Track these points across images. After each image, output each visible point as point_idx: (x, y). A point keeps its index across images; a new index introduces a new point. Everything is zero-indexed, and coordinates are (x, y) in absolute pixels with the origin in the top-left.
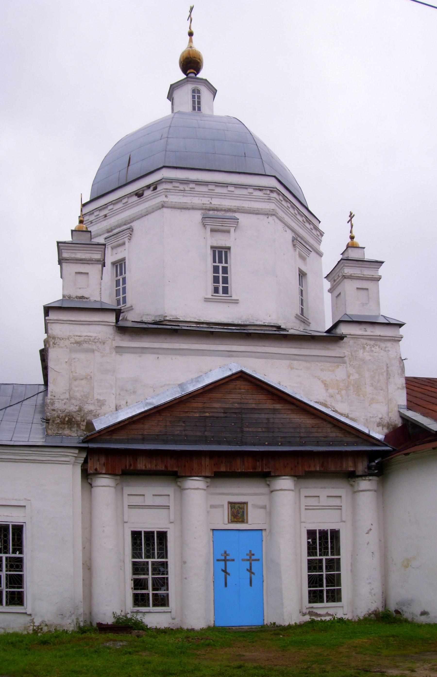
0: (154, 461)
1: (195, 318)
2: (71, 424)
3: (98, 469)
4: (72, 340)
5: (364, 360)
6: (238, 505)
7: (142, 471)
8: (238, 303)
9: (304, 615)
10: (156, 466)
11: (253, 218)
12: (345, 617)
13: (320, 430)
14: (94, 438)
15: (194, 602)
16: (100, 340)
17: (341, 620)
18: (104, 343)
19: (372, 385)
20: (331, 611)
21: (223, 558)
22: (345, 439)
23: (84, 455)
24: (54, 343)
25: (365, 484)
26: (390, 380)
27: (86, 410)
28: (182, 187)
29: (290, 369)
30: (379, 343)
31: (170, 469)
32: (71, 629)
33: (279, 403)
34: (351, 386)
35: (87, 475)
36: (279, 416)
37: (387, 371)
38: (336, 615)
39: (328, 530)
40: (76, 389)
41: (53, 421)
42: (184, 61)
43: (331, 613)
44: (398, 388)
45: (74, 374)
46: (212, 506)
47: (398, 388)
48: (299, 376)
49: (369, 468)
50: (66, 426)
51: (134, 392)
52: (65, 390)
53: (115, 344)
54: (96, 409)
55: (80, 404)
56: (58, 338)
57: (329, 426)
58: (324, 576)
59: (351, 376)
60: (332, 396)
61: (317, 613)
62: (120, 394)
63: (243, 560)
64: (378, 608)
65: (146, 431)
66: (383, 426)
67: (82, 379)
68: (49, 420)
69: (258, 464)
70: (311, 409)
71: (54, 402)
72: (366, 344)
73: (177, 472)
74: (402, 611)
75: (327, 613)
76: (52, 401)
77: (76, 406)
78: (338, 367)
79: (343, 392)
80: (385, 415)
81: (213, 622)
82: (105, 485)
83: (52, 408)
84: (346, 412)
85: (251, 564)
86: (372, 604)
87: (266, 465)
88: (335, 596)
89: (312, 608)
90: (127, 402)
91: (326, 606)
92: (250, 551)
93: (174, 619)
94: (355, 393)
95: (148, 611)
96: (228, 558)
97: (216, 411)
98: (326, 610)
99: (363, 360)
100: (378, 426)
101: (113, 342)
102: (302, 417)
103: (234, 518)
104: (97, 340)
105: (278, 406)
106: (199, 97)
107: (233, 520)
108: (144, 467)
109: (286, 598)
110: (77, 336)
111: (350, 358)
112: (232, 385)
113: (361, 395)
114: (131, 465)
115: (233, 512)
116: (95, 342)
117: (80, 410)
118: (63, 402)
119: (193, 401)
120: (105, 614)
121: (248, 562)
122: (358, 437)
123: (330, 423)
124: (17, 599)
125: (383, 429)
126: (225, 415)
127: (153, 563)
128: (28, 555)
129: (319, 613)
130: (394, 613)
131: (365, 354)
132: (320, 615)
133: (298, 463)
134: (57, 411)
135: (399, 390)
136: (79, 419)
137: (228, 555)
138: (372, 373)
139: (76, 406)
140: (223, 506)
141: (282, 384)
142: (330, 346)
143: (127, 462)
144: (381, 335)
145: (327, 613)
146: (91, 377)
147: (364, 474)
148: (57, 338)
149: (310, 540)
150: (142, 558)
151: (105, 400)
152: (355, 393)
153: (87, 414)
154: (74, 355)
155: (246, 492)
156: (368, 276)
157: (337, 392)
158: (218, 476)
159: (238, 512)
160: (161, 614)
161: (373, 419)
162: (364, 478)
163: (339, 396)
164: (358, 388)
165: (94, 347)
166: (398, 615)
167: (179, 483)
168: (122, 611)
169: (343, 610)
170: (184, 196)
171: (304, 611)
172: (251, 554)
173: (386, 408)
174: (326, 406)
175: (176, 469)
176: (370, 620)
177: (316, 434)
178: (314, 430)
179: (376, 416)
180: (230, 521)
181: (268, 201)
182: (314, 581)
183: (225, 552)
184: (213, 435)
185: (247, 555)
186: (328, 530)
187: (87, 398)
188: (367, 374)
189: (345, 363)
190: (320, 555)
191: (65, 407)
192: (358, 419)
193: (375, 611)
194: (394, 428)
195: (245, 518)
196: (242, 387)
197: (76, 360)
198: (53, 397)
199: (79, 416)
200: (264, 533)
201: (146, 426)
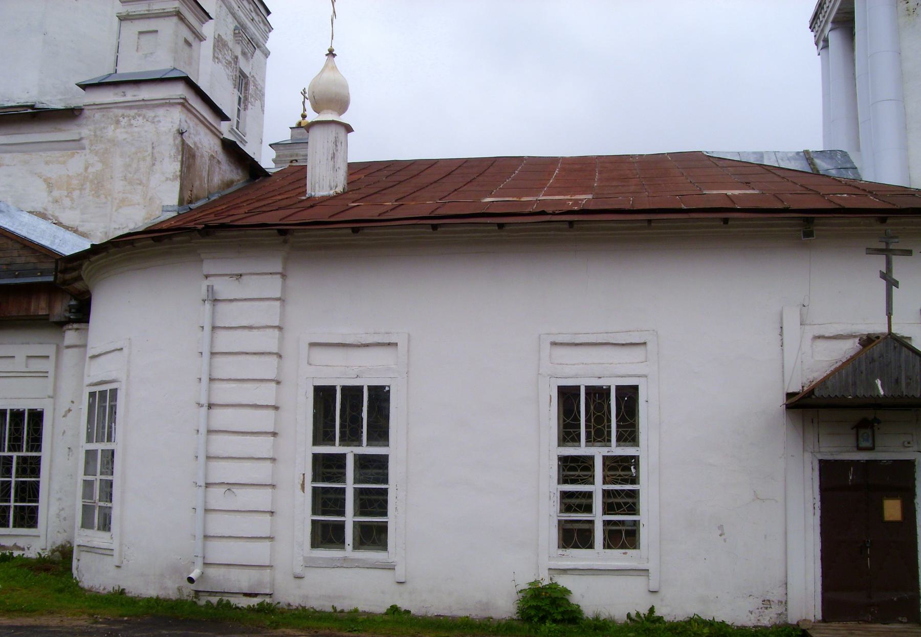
19: (125, 178)
20: (21, 543)
30: (144, 111)
44: (167, 179)
47: (167, 179)
48: (9, 176)
58: (13, 485)
78: (73, 155)
79: (76, 194)
99: (113, 142)
113: (102, 196)
124: (28, 518)
128: (397, 450)
131: (118, 130)
135: (169, 182)
138: (128, 160)
142: (63, 126)
145: (15, 545)
163: (68, 199)
164: (98, 185)
182: (327, 501)
189: (84, 148)
190: (10, 450)
193: (63, 546)
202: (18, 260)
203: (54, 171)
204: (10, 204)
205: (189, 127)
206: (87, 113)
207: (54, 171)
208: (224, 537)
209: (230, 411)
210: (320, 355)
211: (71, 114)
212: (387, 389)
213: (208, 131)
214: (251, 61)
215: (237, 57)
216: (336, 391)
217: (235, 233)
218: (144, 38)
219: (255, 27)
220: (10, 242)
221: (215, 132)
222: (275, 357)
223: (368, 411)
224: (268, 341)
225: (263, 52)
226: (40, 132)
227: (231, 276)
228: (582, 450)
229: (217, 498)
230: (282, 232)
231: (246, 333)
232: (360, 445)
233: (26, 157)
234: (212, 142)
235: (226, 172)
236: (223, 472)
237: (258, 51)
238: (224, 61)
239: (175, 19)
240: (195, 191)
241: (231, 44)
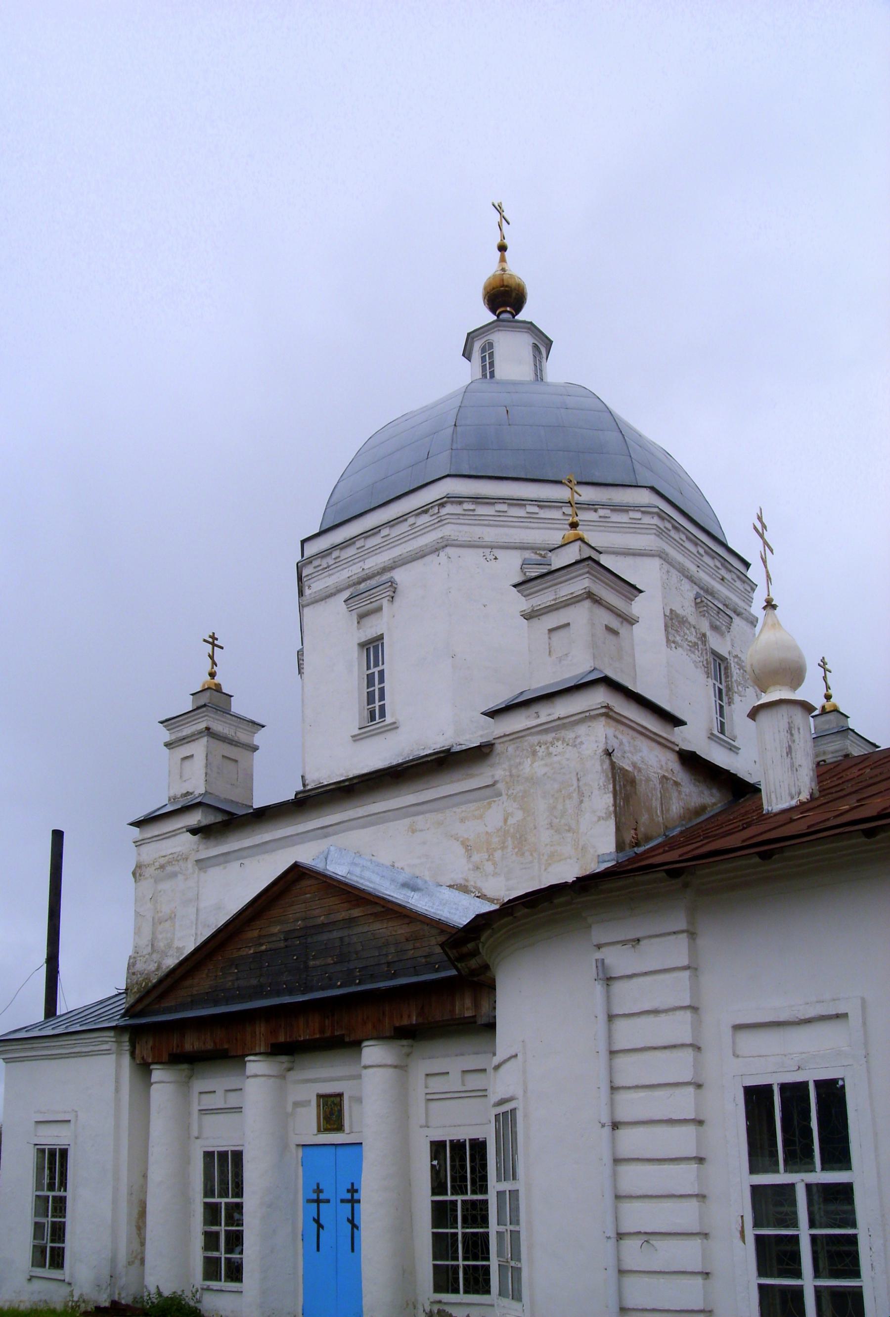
1: (342, 775)
4: (157, 865)
5: (532, 779)
6: (332, 1099)
8: (397, 728)
11: (417, 567)
18: (187, 859)
24: (140, 875)
28: (324, 563)
30: (563, 733)
35: (144, 1068)
36: (360, 929)
42: (488, 301)
44: (600, 818)
45: (160, 915)
48: (424, 843)
63: (342, 1201)
69: (327, 1021)
72: (539, 743)
73: (227, 1050)
79: (498, 854)
94: (516, 850)
97: (274, 939)
99: (532, 780)
105: (356, 912)
106: (491, 355)
113: (527, 854)
121: (350, 1205)
128: (862, 1174)
131: (536, 764)
135: (602, 822)
137: (321, 1191)
140: (309, 1102)
144: (561, 716)
149: (435, 1163)
150: (214, 1197)
152: (516, 850)
155: (322, 1075)
156: (564, 599)
158: (288, 1050)
163: (490, 863)
165: (177, 868)
170: (330, 575)
175: (226, 1046)
178: (410, 946)
181: (440, 524)
182: (443, 1246)
185: (348, 1191)
189: (500, 794)
203: (472, 829)
204: (428, 879)
205: (621, 743)
206: (499, 748)
207: (472, 829)
208: (646, 1310)
209: (640, 1130)
210: (750, 1042)
211: (481, 753)
212: (841, 1083)
213: (654, 745)
214: (728, 637)
215: (704, 635)
216: (772, 1091)
217: (621, 883)
218: (556, 636)
219: (730, 588)
220: (426, 928)
221: (664, 744)
222: (690, 1050)
223: (819, 1119)
224: (678, 1028)
225: (747, 620)
226: (452, 782)
227: (624, 943)
228: (781, 1178)
229: (634, 1254)
230: (674, 873)
231: (651, 1019)
232: (813, 1170)
233: (439, 816)
234: (663, 759)
235: (692, 795)
236: (638, 1217)
237: (737, 620)
238: (685, 644)
239: (587, 604)
240: (642, 829)
241: (692, 620)
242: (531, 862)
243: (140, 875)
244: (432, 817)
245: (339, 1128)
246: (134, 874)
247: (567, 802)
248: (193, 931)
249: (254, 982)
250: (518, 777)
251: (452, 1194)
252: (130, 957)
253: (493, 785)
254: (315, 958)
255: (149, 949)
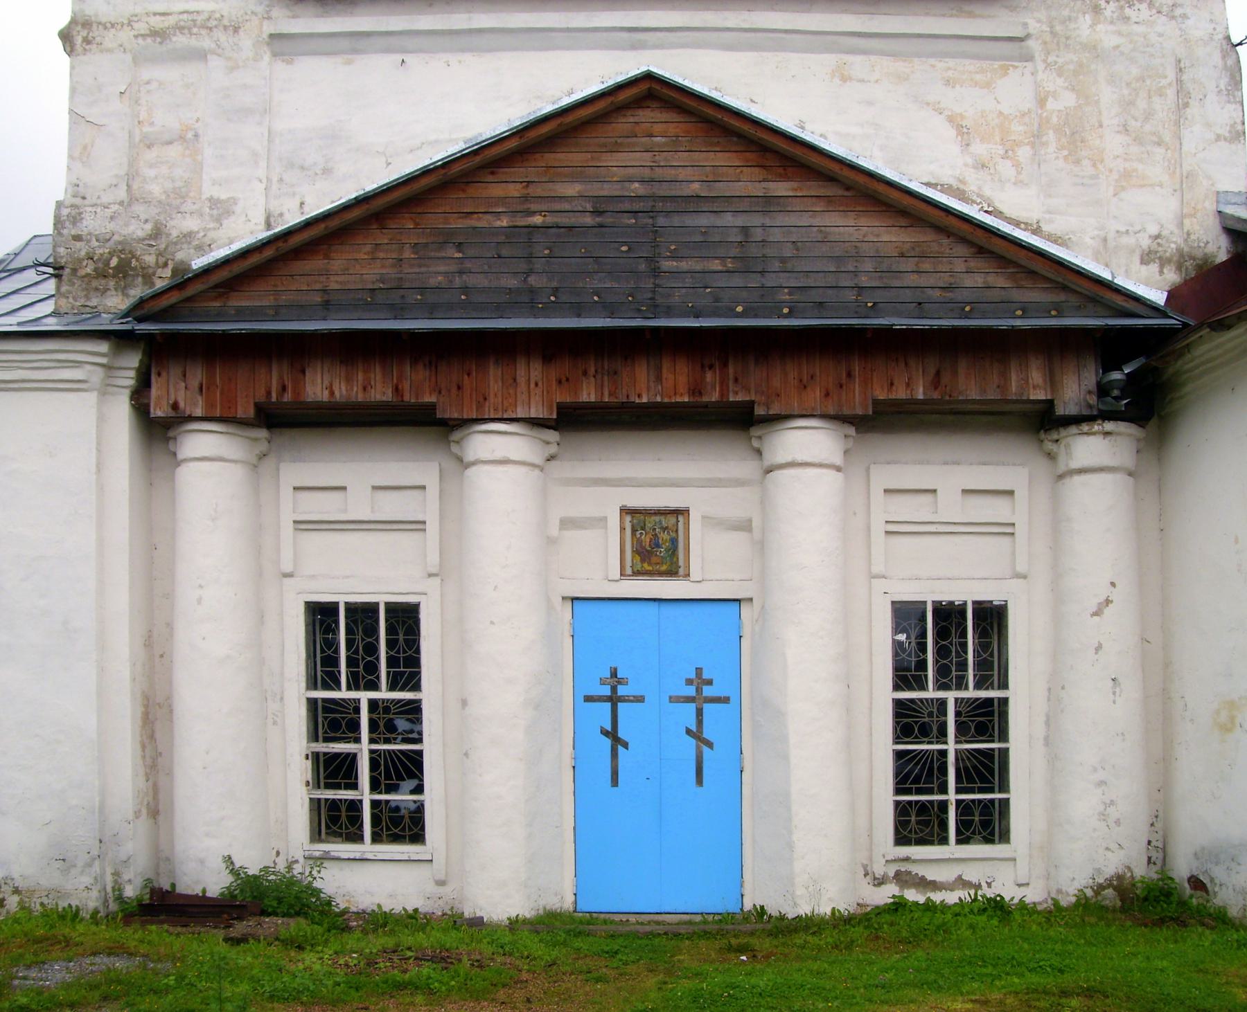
0: (360, 376)
2: (124, 277)
3: (182, 405)
4: (141, 27)
5: (1095, 47)
6: (657, 518)
7: (319, 406)
9: (879, 882)
10: (365, 389)
12: (1010, 893)
13: (927, 266)
14: (172, 306)
15: (501, 834)
16: (226, 22)
17: (997, 907)
18: (236, 30)
19: (1125, 129)
21: (606, 691)
22: (1017, 295)
23: (133, 360)
24: (87, 41)
25: (1088, 447)
26: (1188, 111)
27: (175, 233)
29: (837, 81)
31: (409, 398)
32: (92, 905)
33: (785, 177)
34: (1051, 132)
35: (157, 430)
36: (781, 220)
37: (1179, 82)
38: (989, 885)
39: (965, 603)
40: (151, 173)
41: (74, 271)
43: (974, 880)
44: (1218, 138)
45: (146, 129)
46: (568, 523)
47: (1218, 138)
48: (870, 103)
49: (1103, 390)
50: (112, 283)
51: (327, 171)
52: (116, 176)
53: (269, 28)
54: (205, 229)
55: (159, 214)
56: (100, 23)
57: (961, 250)
59: (1050, 99)
60: (983, 166)
61: (923, 878)
62: (281, 180)
63: (673, 699)
64: (1129, 868)
65: (332, 278)
66: (1163, 262)
67: (170, 143)
68: (62, 268)
70: (895, 195)
71: (81, 213)
73: (432, 407)
74: (1212, 880)
75: (960, 877)
76: (73, 212)
77: (146, 221)
78: (1005, 71)
79: (1024, 153)
80: (1170, 227)
81: (570, 899)
82: (212, 459)
83: (73, 232)
84: (1032, 215)
85: (700, 713)
86: (1109, 854)
87: (736, 380)
88: (986, 824)
89: (907, 859)
90: (302, 204)
91: (956, 856)
92: (699, 671)
93: (441, 883)
95: (358, 856)
96: (622, 690)
97: (567, 207)
98: (369, 879)
99: (1092, 48)
100: (1144, 262)
101: (266, 23)
102: (863, 221)
103: (643, 561)
104: (215, 23)
105: (781, 188)
107: (639, 567)
108: (326, 393)
109: (815, 824)
110: (155, 14)
111: (1045, 43)
112: (623, 124)
113: (1085, 162)
114: (284, 388)
115: (640, 541)
116: (211, 29)
117: (157, 233)
118: (108, 212)
119: (490, 178)
120: (202, 862)
121: (692, 707)
122: (1064, 288)
123: (963, 240)
125: (1161, 272)
126: (598, 220)
127: (373, 704)
129: (929, 878)
130: (1187, 885)
131: (1100, 27)
132: (924, 884)
133: (849, 375)
134: (89, 241)
135: (1222, 143)
136: (150, 259)
137: (621, 682)
138: (1126, 92)
139: (146, 221)
141: (807, 126)
143: (270, 382)
145: (960, 877)
146: (196, 136)
147: (1085, 412)
148: (95, 26)
151: (234, 201)
152: (1066, 153)
153: (176, 244)
154: (147, 73)
157: (1002, 152)
159: (655, 542)
160: (402, 864)
161: (1125, 240)
162: (1085, 427)
163: (1008, 163)
164: (1074, 137)
165: (207, 43)
166: (1199, 893)
167: (454, 448)
168: (278, 853)
169: (1015, 871)
171: (879, 869)
172: (700, 680)
173: (1173, 204)
174: (962, 196)
175: (429, 398)
176: (1104, 908)
177: (915, 276)
178: (909, 265)
179: (1138, 228)
180: (629, 571)
182: (913, 773)
183: (614, 673)
184: (555, 284)
185: (689, 682)
186: (965, 603)
187: (182, 197)
188: (1107, 95)
189: (1029, 58)
191: (111, 226)
192: (1074, 238)
193: (1120, 877)
194: (1199, 267)
195: (681, 563)
196: (658, 128)
197: (154, 85)
198: (78, 201)
199: (152, 250)
200: (745, 608)
201: (337, 264)
202: (968, 281)
203: (970, 102)
233: (900, 66)
242: (1095, 177)
243: (87, 41)
244: (886, 63)
245: (672, 571)
246: (66, 37)
247: (1156, 99)
248: (261, 172)
249: (513, 283)
250: (1067, 38)
251: (349, 688)
252: (59, 205)
253: (1021, 40)
254: (674, 256)
255: (122, 194)
